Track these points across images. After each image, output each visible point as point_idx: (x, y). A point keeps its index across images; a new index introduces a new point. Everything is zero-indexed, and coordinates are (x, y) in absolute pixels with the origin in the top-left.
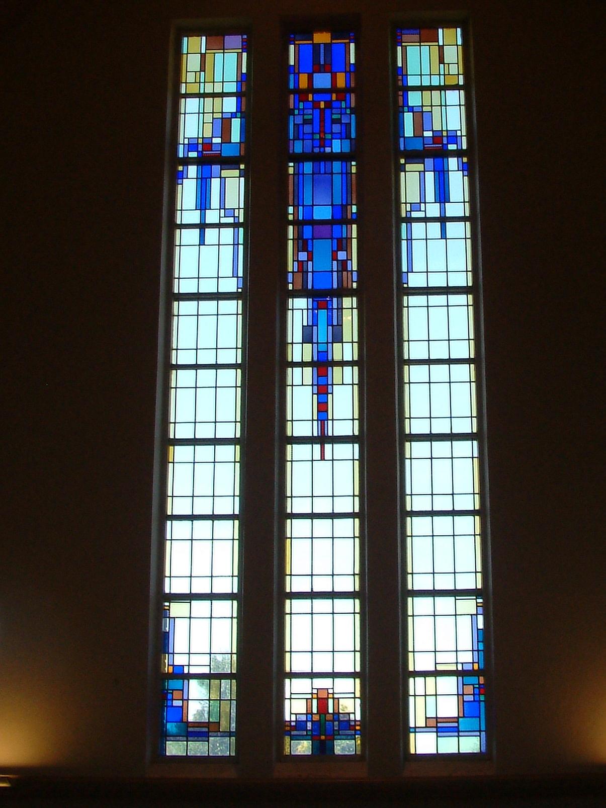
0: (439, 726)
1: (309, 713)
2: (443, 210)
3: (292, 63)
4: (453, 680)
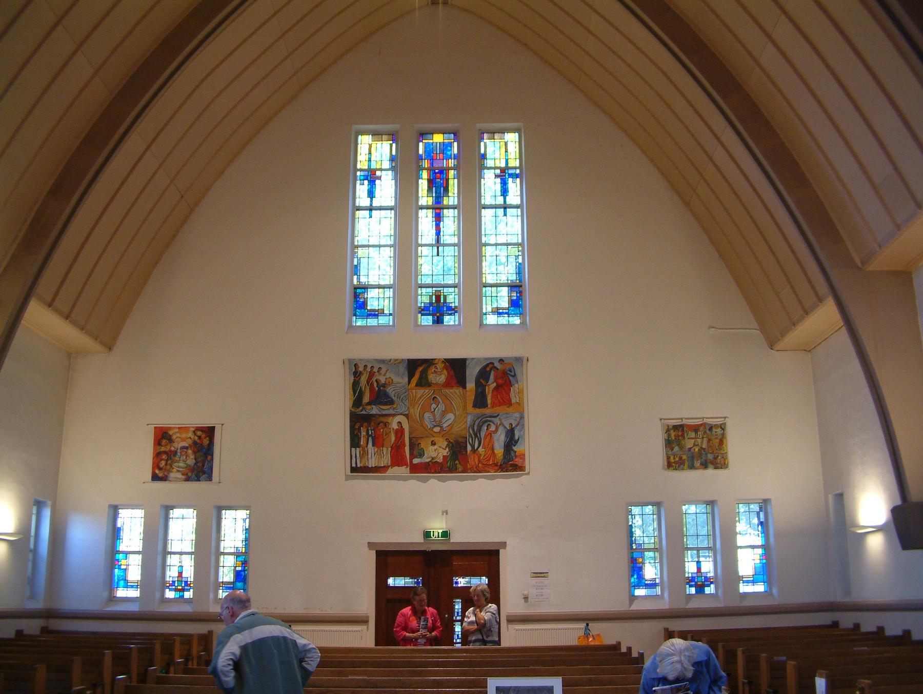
0: (498, 312)
4: (506, 289)
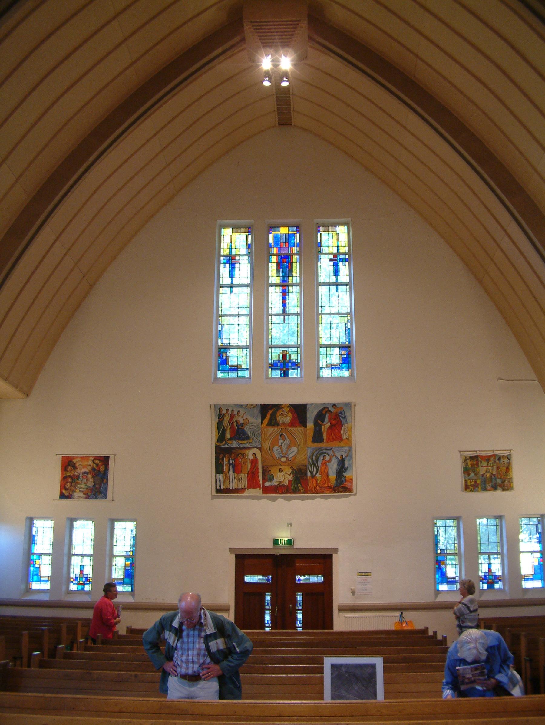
0: (331, 367)
1: (279, 360)
2: (337, 280)
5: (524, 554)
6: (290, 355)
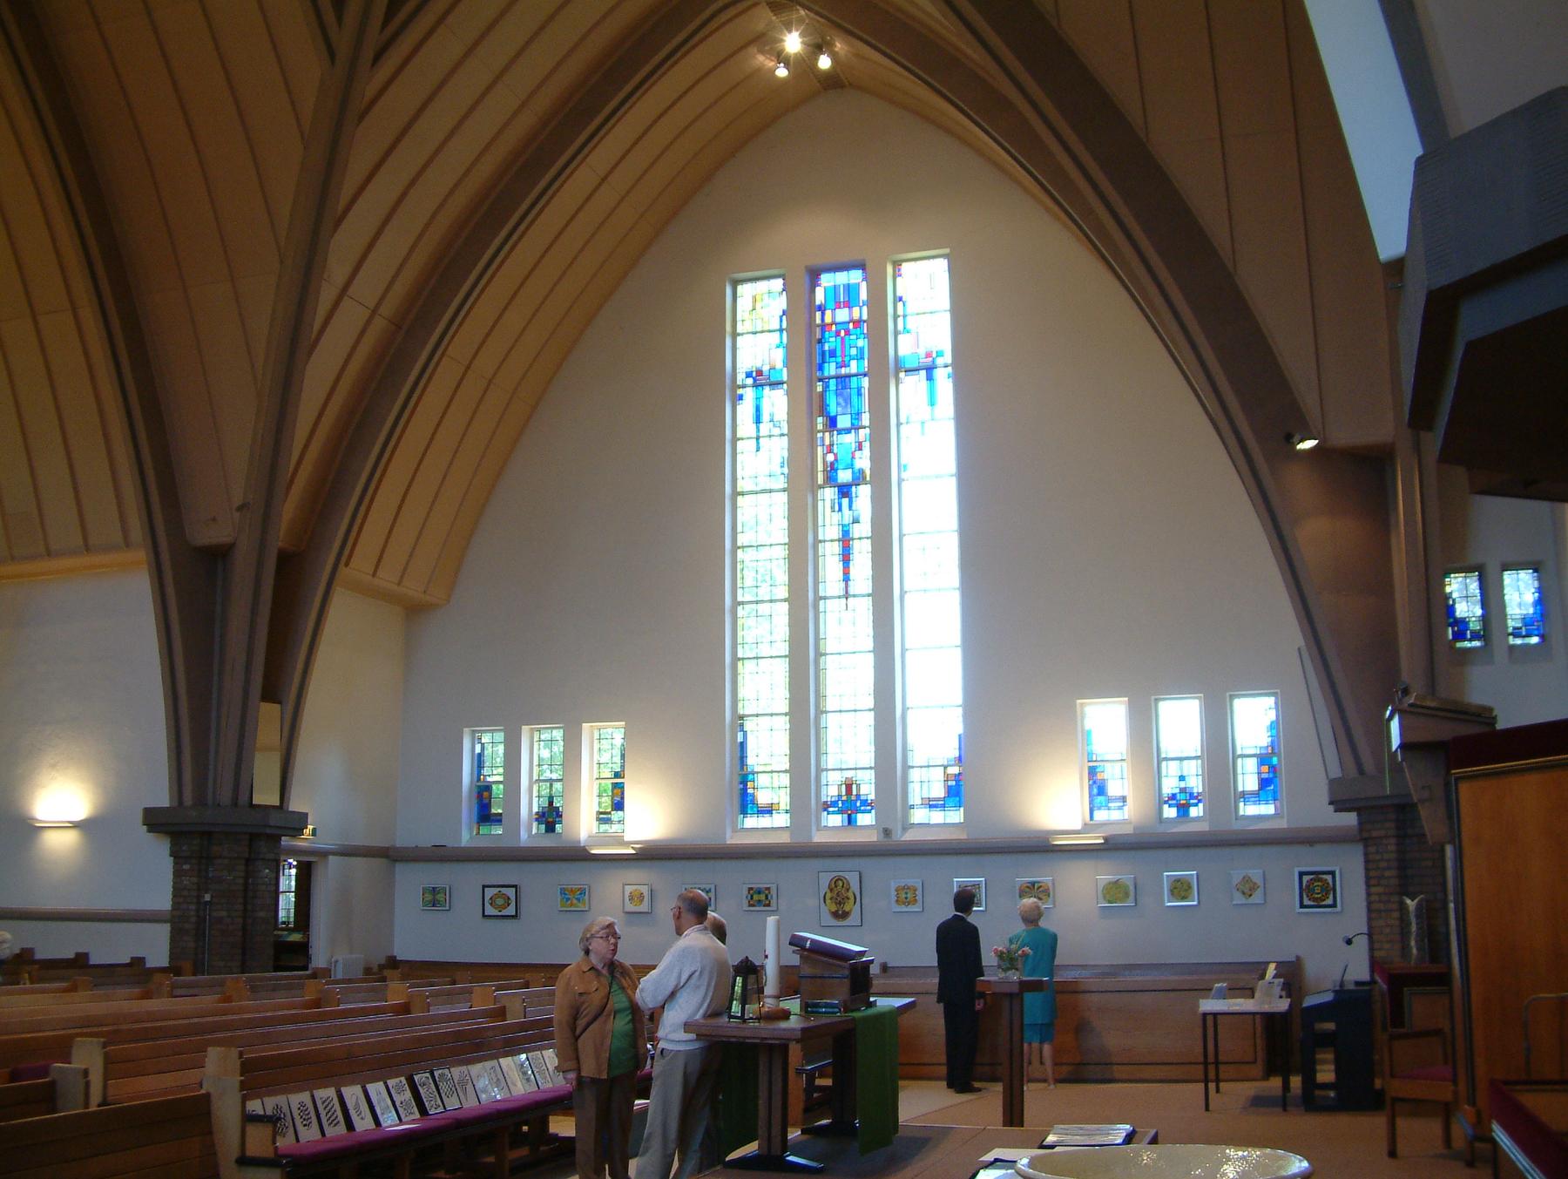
0: (931, 804)
1: (840, 796)
3: (1496, 1127)
5: (248, 1145)
6: (858, 786)
